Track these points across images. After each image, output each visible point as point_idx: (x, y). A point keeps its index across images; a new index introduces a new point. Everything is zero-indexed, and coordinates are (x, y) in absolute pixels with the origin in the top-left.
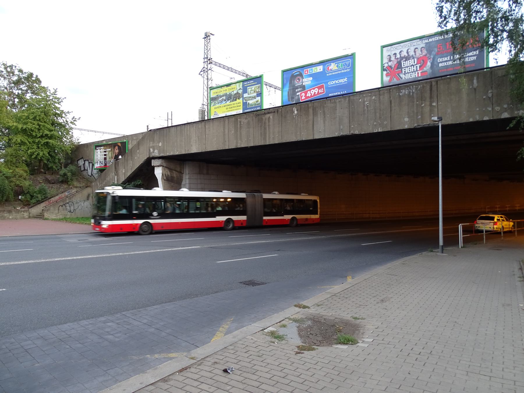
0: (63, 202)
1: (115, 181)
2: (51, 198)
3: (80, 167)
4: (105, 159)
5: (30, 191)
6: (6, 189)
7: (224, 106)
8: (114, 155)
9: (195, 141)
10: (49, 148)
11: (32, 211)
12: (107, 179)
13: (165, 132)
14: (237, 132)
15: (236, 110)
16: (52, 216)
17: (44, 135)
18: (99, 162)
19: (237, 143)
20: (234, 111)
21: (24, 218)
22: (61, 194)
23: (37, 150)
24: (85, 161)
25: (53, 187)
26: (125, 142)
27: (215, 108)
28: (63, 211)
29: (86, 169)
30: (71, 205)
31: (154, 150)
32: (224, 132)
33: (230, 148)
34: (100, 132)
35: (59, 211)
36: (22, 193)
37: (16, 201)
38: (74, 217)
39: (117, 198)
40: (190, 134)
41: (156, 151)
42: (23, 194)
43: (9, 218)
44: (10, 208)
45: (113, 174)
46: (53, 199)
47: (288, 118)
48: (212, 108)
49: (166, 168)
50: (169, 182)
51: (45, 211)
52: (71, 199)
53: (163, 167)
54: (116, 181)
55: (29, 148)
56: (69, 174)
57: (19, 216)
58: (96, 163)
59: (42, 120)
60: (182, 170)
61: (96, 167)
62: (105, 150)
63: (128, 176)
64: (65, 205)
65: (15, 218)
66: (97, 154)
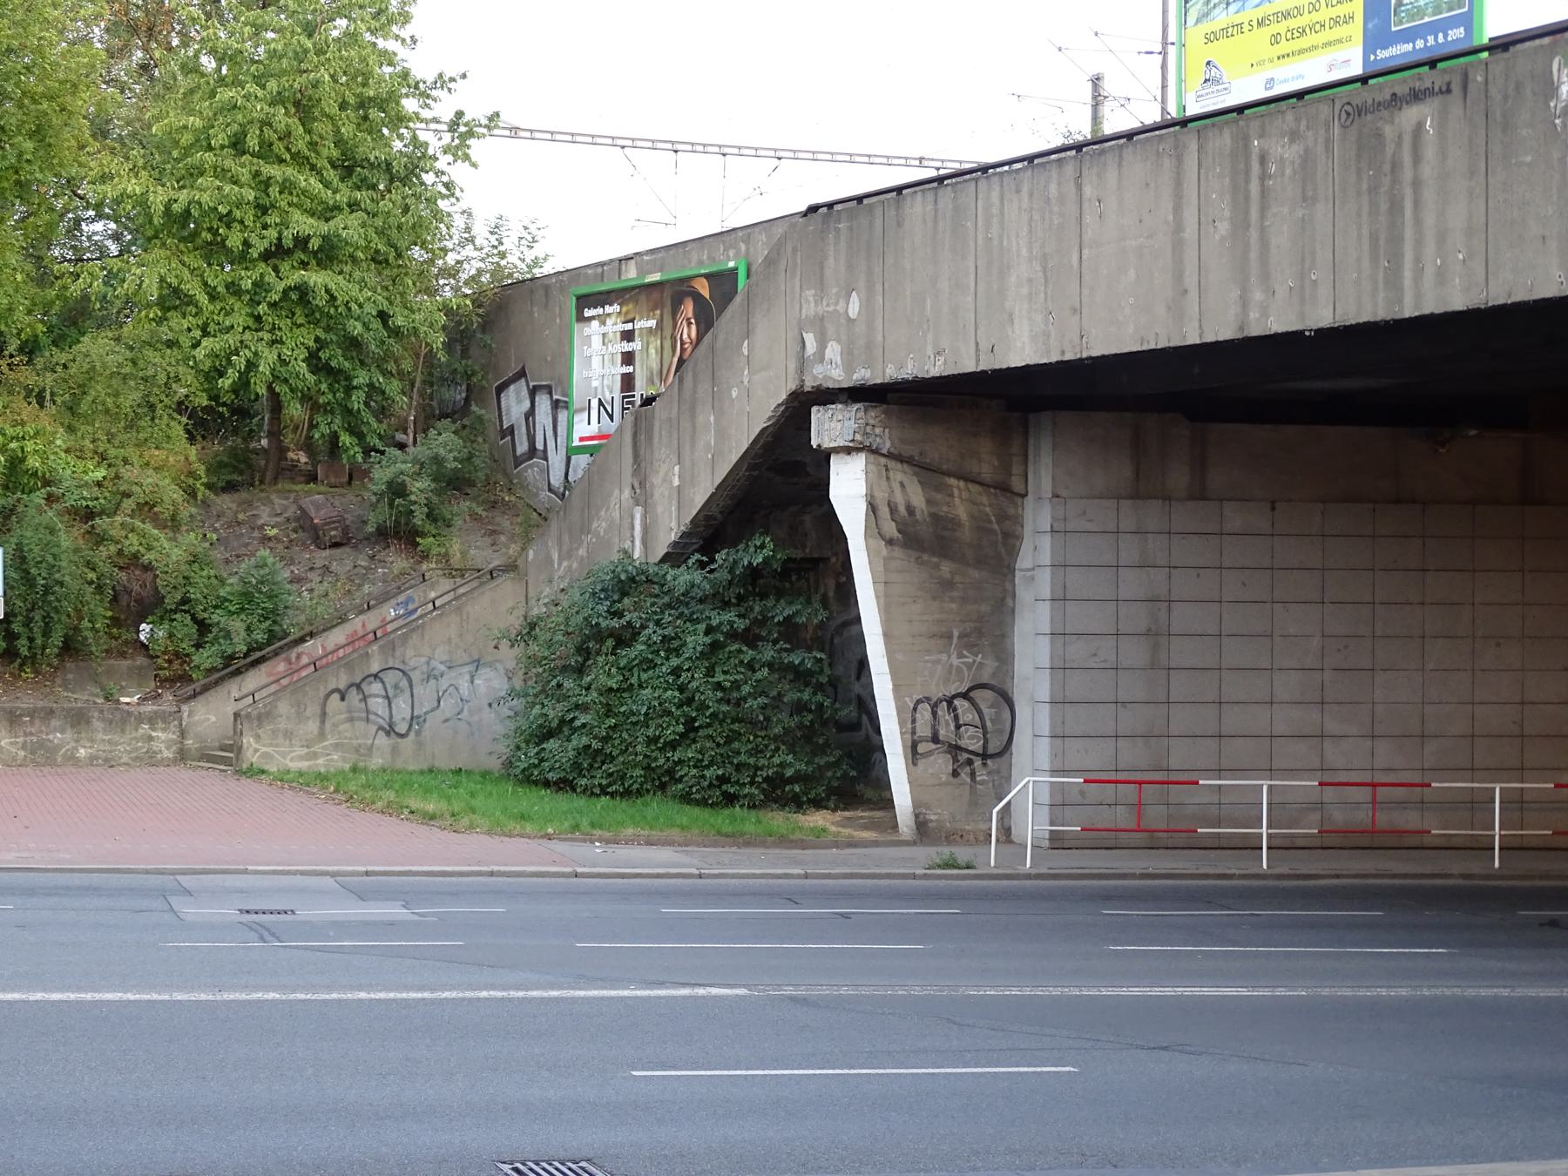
0: (349, 666)
1: (633, 542)
2: (302, 640)
3: (511, 430)
4: (628, 382)
5: (194, 594)
6: (61, 584)
7: (1260, 24)
8: (676, 360)
9: (1025, 291)
10: (317, 323)
11: (196, 718)
12: (595, 525)
13: (878, 222)
14: (1248, 227)
15: (1325, 45)
16: (284, 755)
17: (288, 242)
18: (595, 403)
19: (1244, 303)
20: (1314, 53)
21: (150, 760)
22: (362, 617)
23: (247, 335)
24: (533, 392)
25: (334, 566)
26: (733, 273)
27: (1210, 38)
28: (348, 725)
29: (540, 446)
30: (396, 687)
31: (822, 345)
32: (1179, 227)
33: (1210, 338)
34: (757, 153)
35: (328, 725)
36: (149, 607)
37: (123, 655)
38: (411, 768)
39: (854, 630)
40: (1001, 237)
41: (833, 351)
42: (159, 612)
43: (72, 759)
44: (82, 697)
45: (627, 493)
46: (313, 648)
47: (1524, 132)
48: (1195, 34)
49: (892, 464)
50: (925, 557)
51: (246, 725)
52: (398, 653)
53: (872, 457)
54: (638, 543)
55: (212, 328)
56: (420, 488)
57: (123, 744)
58: (582, 410)
59: (279, 148)
60: (1016, 469)
61: (582, 439)
62: (629, 326)
63: (694, 512)
64: (358, 686)
65: (106, 760)
66: (587, 352)
